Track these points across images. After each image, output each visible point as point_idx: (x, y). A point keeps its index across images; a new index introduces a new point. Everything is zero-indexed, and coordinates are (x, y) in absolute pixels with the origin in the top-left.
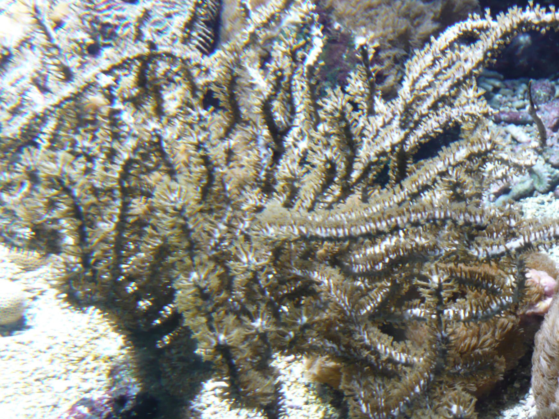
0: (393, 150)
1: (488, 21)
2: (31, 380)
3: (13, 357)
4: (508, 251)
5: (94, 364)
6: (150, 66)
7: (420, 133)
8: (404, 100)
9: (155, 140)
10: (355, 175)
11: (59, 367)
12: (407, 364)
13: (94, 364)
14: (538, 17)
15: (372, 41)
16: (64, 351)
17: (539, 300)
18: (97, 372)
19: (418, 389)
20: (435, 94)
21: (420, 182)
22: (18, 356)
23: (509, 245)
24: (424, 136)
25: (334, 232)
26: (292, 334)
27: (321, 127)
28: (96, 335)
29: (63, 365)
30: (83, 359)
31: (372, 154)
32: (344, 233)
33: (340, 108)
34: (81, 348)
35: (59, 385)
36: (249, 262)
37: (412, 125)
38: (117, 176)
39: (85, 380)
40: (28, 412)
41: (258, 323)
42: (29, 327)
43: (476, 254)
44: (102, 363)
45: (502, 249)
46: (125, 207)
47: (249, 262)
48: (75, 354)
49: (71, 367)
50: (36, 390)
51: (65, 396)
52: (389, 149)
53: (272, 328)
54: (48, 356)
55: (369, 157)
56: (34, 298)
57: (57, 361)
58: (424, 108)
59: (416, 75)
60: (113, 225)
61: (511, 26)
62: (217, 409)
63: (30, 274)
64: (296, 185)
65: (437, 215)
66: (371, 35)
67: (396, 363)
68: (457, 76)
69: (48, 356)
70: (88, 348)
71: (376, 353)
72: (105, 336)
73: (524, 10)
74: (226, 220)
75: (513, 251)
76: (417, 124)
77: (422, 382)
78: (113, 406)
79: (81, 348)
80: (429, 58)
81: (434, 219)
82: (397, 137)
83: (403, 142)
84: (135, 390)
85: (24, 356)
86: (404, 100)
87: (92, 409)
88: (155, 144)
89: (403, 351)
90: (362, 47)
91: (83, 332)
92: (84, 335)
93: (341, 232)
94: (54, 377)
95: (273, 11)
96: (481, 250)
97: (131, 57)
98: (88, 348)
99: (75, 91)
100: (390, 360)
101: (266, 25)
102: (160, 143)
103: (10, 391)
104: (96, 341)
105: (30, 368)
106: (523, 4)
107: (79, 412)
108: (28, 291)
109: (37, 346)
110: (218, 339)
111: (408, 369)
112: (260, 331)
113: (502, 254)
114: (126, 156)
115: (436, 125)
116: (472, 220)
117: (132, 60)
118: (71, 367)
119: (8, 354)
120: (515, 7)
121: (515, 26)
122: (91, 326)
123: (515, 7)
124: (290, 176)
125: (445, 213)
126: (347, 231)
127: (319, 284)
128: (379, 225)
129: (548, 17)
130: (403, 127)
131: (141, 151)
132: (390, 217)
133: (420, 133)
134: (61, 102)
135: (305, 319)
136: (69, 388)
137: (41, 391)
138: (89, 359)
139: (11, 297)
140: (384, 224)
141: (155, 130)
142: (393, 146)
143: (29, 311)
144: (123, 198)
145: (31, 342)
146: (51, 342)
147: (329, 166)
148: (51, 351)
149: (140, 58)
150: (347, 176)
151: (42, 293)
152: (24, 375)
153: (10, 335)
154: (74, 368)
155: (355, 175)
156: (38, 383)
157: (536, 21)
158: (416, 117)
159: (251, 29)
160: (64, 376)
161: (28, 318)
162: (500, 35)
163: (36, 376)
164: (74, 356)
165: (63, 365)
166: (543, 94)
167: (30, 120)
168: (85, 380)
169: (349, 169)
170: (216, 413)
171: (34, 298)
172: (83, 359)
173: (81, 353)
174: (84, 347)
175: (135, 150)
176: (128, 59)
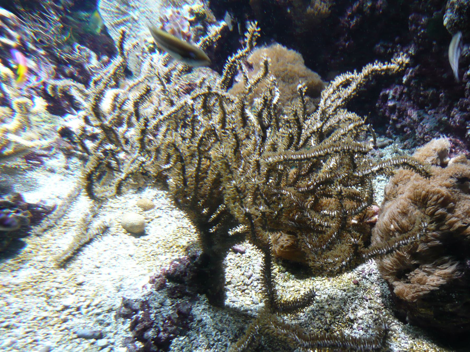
0: (318, 130)
1: (355, 75)
2: (150, 255)
3: (141, 246)
4: (372, 172)
5: (176, 249)
6: (208, 99)
7: (328, 125)
8: (322, 108)
9: (213, 129)
10: (301, 143)
11: (161, 250)
12: (327, 227)
13: (176, 249)
14: (380, 67)
15: (304, 87)
16: (163, 243)
17: (373, 216)
18: (178, 252)
19: (334, 236)
20: (335, 105)
21: (333, 139)
22: (144, 246)
23: (372, 170)
24: (330, 126)
25: (299, 156)
26: (276, 212)
27: (281, 130)
28: (177, 237)
29: (163, 249)
30: (172, 247)
31: (308, 133)
32: (304, 157)
33: (295, 110)
34: (170, 242)
35: (162, 258)
36: (255, 181)
37: (326, 119)
38: (197, 145)
39: (173, 256)
40: (149, 268)
41: (261, 208)
42: (147, 235)
43: (357, 175)
44: (180, 249)
45: (370, 171)
46: (200, 161)
47: (255, 181)
48: (168, 245)
49: (166, 250)
50: (152, 259)
51: (165, 262)
52: (316, 130)
53: (268, 210)
54: (157, 245)
55: (307, 134)
56: (149, 222)
57: (161, 248)
58: (331, 111)
59: (326, 97)
60: (195, 169)
61: (368, 72)
62: (232, 268)
63: (147, 212)
64: (276, 146)
65: (345, 148)
66: (304, 84)
67: (322, 226)
68: (345, 96)
69: (157, 245)
70: (174, 242)
71: (314, 222)
72: (181, 238)
73: (373, 65)
74: (242, 167)
75: (375, 172)
76: (328, 118)
77: (336, 233)
78: (190, 260)
79: (170, 242)
80: (331, 90)
81: (344, 150)
82: (319, 125)
83: (322, 127)
84: (200, 253)
85: (146, 245)
86: (322, 108)
87: (181, 262)
88: (213, 130)
89: (326, 221)
90: (300, 89)
91: (171, 236)
92: (172, 237)
93: (303, 156)
94: (159, 254)
95: (259, 77)
96: (360, 173)
97: (201, 94)
98: (174, 242)
99: (177, 109)
100: (320, 225)
101: (256, 84)
102: (214, 130)
103: (141, 260)
104: (177, 240)
105: (149, 250)
106: (372, 62)
107: (175, 264)
108: (146, 219)
109: (151, 241)
110: (246, 210)
111: (328, 229)
112: (262, 211)
113: (370, 173)
114: (201, 136)
115: (334, 122)
116: (361, 149)
117: (201, 95)
118: (166, 250)
119: (140, 244)
120: (369, 64)
121: (370, 72)
122: (174, 233)
123: (369, 64)
124: (273, 143)
125: (349, 147)
126: (305, 156)
127: (285, 195)
128: (319, 153)
129: (385, 67)
130: (321, 120)
131: (207, 133)
132: (325, 149)
133: (328, 125)
134: (171, 114)
135: (282, 205)
136: (167, 259)
137: (154, 260)
138: (174, 247)
139: (139, 221)
140: (322, 152)
141: (212, 124)
142: (318, 129)
143: (147, 228)
144: (199, 156)
145: (149, 240)
146: (158, 240)
147: (291, 136)
148: (158, 243)
149: (204, 95)
150: (298, 143)
151: (152, 220)
152: (147, 253)
153: (139, 237)
154: (168, 251)
155: (301, 143)
156: (153, 257)
157: (379, 69)
158: (327, 116)
159: (249, 86)
160: (164, 254)
161: (146, 231)
162: (363, 77)
163: (152, 253)
164: (168, 246)
165: (163, 249)
166: (363, 137)
167: (157, 123)
168: (173, 256)
169: (299, 140)
170: (231, 269)
171: (149, 222)
172: (172, 247)
173: (171, 244)
174: (172, 242)
175: (204, 133)
176: (199, 95)
